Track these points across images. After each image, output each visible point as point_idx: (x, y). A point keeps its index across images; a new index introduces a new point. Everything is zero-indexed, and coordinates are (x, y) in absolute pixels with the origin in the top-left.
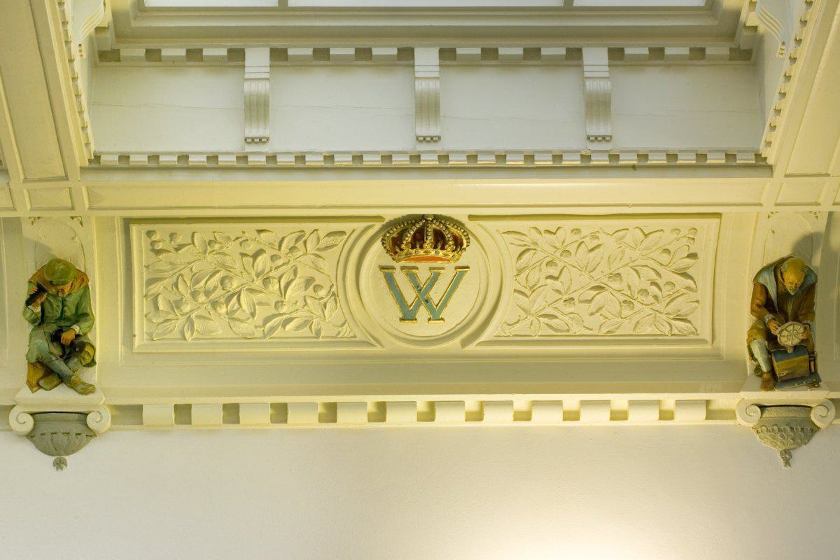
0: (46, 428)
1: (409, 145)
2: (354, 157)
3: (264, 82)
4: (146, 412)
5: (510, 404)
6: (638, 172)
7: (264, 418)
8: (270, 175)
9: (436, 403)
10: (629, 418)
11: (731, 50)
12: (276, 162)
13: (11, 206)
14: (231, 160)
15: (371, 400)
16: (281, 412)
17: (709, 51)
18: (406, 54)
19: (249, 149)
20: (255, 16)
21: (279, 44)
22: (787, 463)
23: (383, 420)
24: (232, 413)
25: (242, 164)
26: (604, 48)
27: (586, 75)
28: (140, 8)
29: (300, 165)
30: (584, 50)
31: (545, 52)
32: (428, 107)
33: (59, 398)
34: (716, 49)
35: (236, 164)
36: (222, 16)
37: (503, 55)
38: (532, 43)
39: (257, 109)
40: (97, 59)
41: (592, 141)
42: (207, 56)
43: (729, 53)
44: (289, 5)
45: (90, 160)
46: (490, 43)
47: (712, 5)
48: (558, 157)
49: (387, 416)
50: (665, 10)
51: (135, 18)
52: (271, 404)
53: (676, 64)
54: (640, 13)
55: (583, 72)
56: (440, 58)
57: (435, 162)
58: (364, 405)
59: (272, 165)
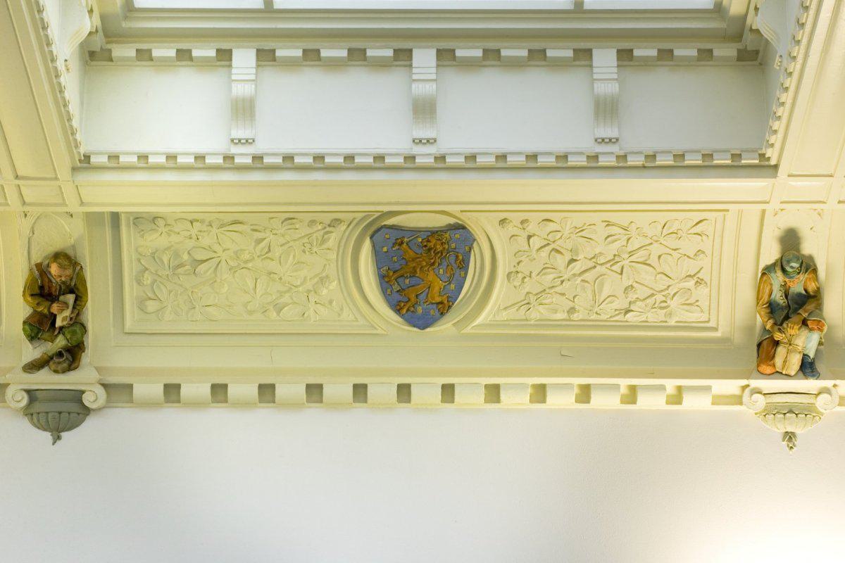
0: (38, 407)
1: (405, 146)
2: (497, 157)
3: (431, 84)
4: (326, 390)
5: (708, 388)
6: (645, 172)
7: (480, 396)
8: (531, 173)
9: (592, 386)
10: (637, 402)
11: (739, 51)
12: (445, 162)
13: (61, 201)
14: (582, 161)
15: (624, 383)
16: (493, 393)
17: (716, 53)
18: (225, 56)
19: (417, 150)
20: (405, 18)
21: (268, 45)
22: (53, 444)
23: (634, 402)
24: (448, 391)
25: (592, 165)
26: (251, 50)
27: (234, 77)
28: (130, 9)
29: (471, 163)
30: (595, 52)
31: (550, 53)
32: (424, 109)
33: (46, 379)
34: (726, 51)
35: (343, 164)
36: (460, 18)
37: (326, 57)
38: (537, 45)
39: (424, 109)
40: (88, 58)
41: (417, 143)
42: (678, 56)
43: (697, 54)
44: (275, 7)
45: (80, 161)
46: (492, 45)
47: (719, 10)
48: (708, 156)
49: (592, 396)
50: (305, 12)
51: (126, 18)
52: (486, 385)
53: (686, 63)
54: (442, 16)
55: (592, 73)
56: (438, 59)
57: (727, 162)
58: (617, 387)
59: (622, 166)
